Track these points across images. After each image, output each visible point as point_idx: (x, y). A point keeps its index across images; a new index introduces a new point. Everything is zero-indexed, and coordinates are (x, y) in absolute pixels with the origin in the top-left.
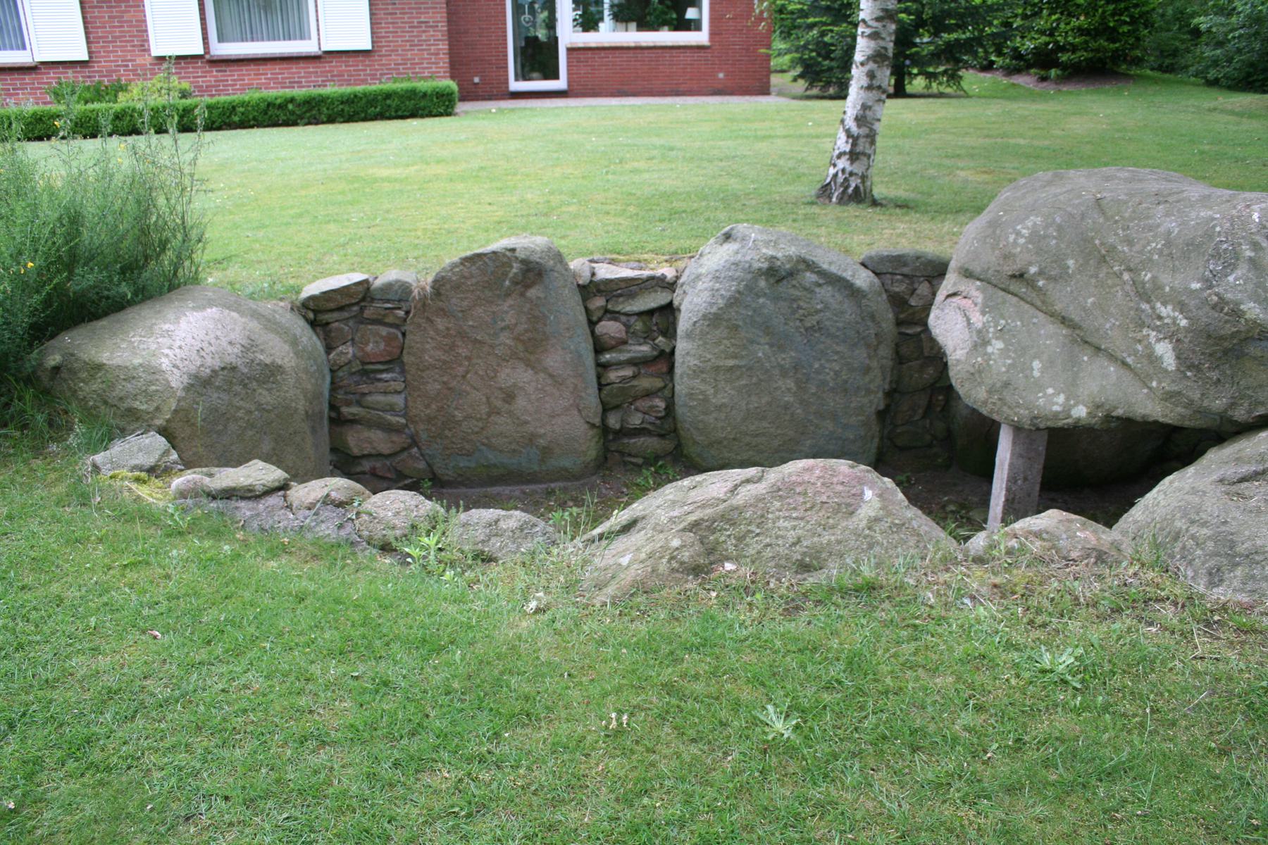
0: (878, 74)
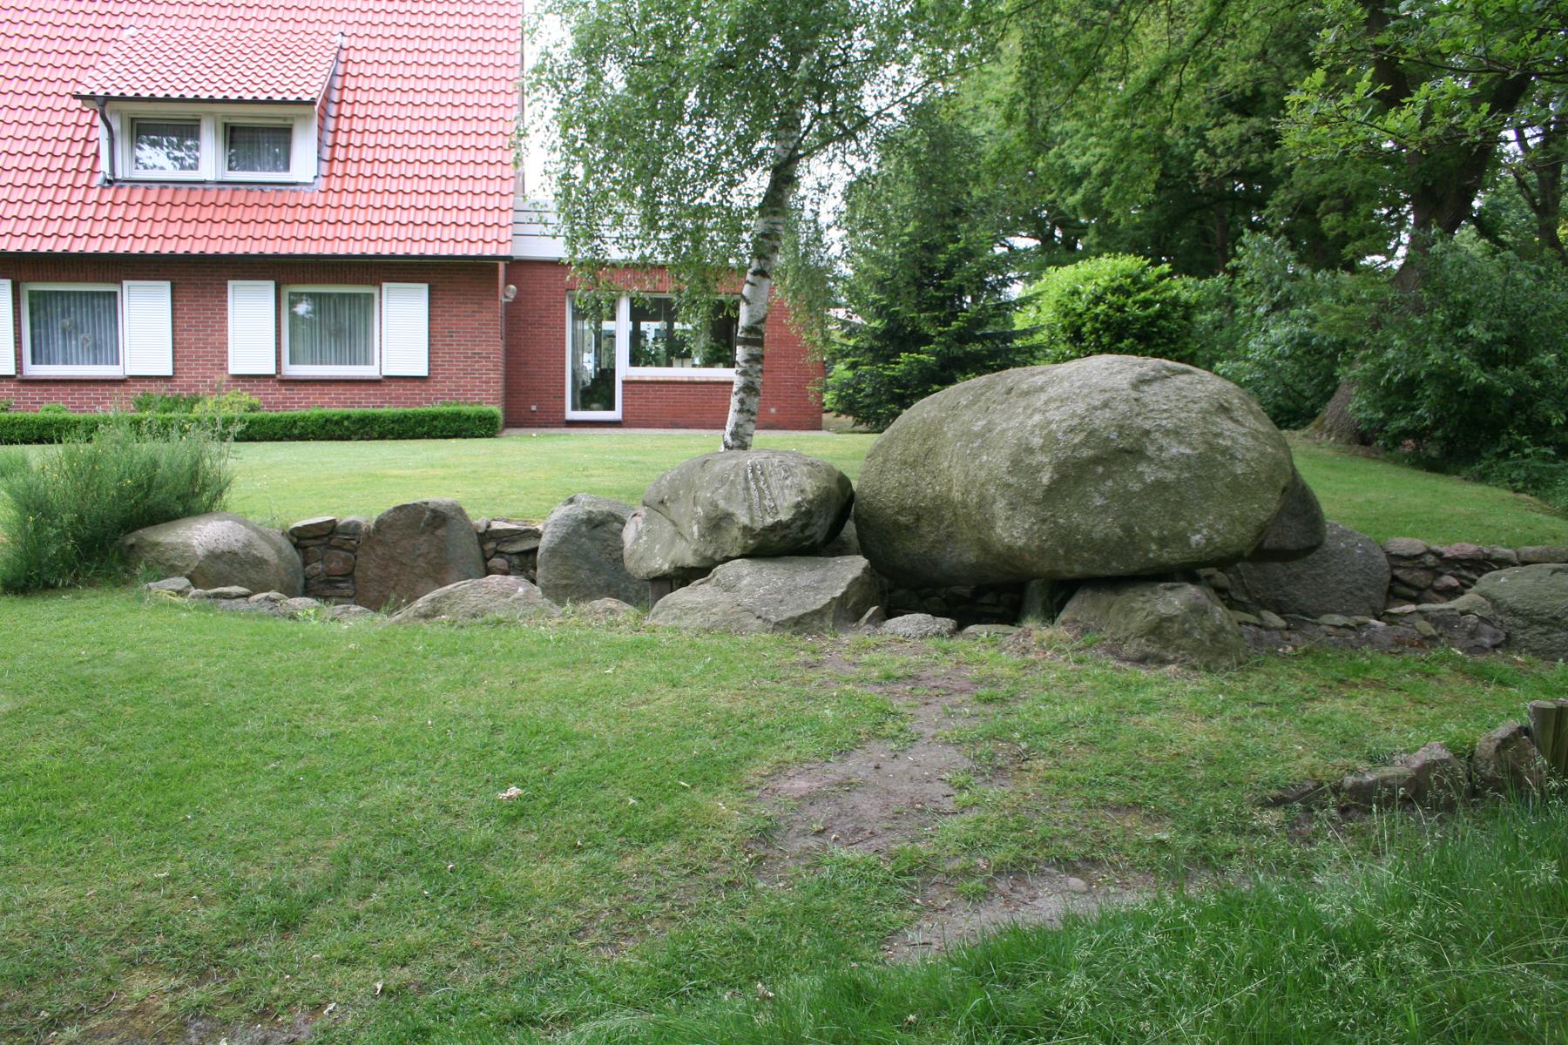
0: (748, 401)
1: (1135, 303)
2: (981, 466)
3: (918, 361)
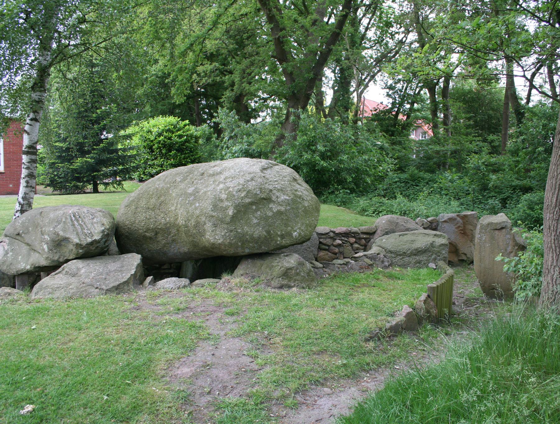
0: (30, 181)
1: (176, 136)
2: (196, 208)
3: (86, 162)
